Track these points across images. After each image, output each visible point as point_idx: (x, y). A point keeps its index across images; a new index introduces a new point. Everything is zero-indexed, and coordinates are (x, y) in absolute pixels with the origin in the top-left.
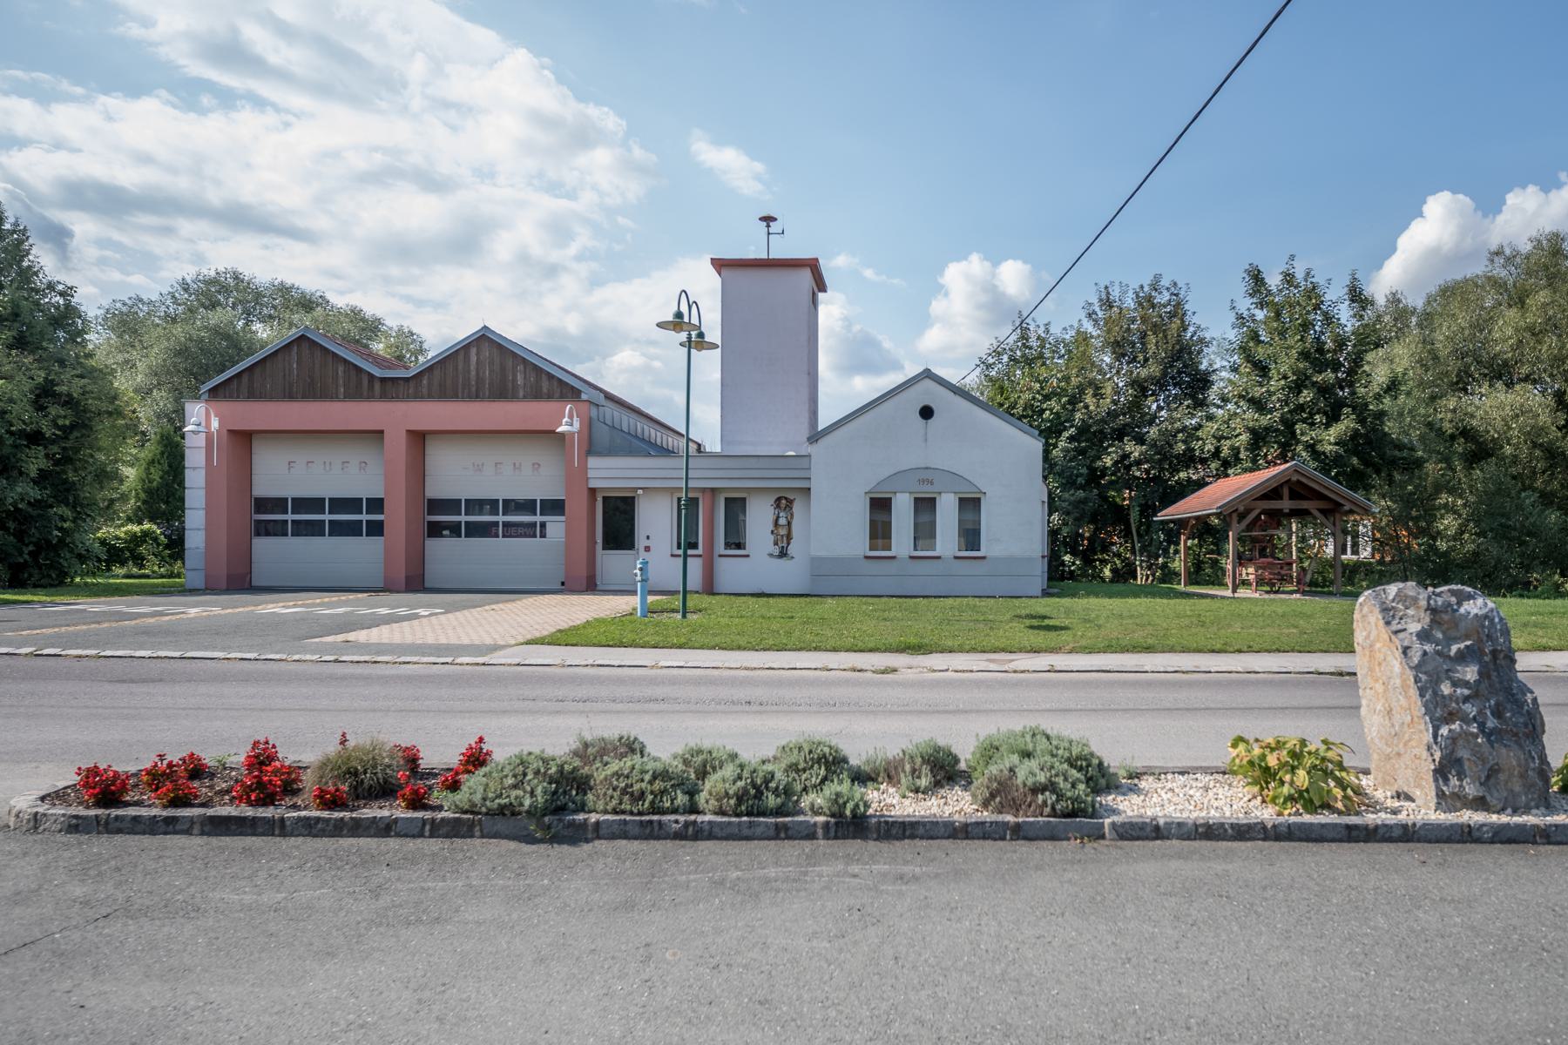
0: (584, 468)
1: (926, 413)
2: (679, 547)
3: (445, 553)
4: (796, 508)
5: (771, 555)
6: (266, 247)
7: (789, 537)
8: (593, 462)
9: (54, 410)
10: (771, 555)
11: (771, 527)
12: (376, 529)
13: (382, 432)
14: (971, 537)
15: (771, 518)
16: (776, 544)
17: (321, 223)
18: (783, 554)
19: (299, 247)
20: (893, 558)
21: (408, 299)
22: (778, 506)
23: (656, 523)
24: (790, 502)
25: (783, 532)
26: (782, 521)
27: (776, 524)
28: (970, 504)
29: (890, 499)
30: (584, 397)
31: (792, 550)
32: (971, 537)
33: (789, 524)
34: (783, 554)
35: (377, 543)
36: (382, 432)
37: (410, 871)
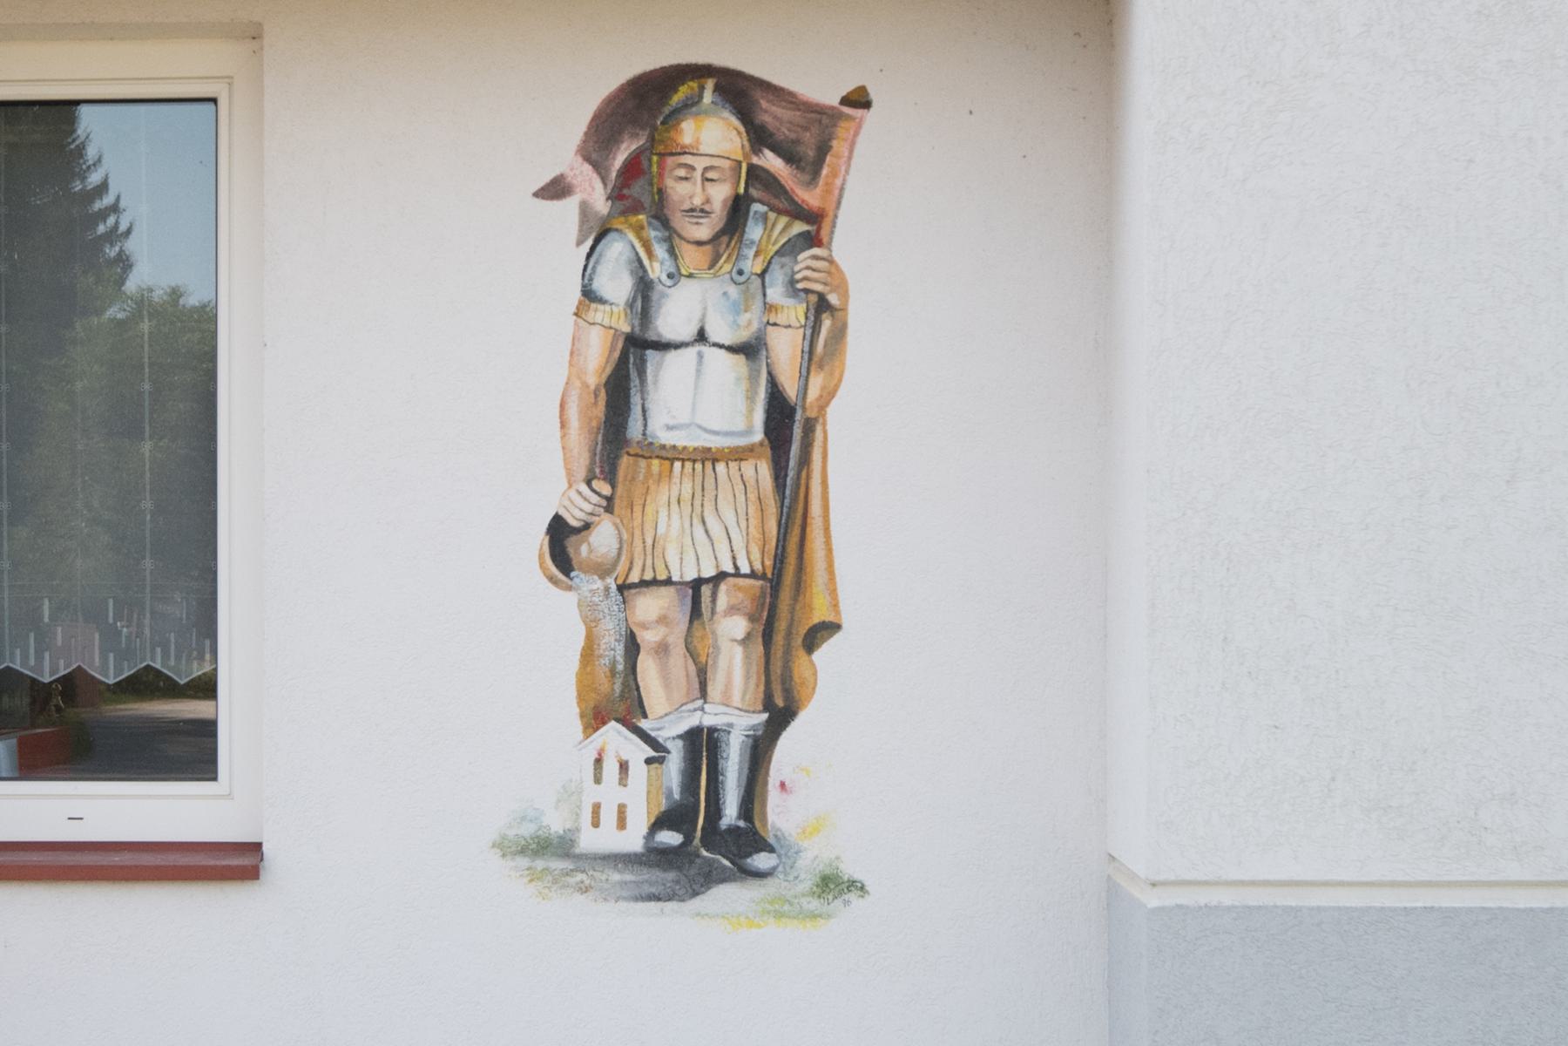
4: (880, 201)
5: (548, 851)
7: (785, 607)
10: (548, 851)
11: (551, 481)
13: (256, 848)
15: (554, 359)
16: (614, 702)
18: (709, 836)
20: (236, 863)
22: (638, 195)
24: (793, 144)
25: (701, 531)
26: (698, 400)
27: (614, 428)
31: (815, 790)
33: (786, 429)
34: (709, 836)
36: (256, 848)
37: (654, 589)
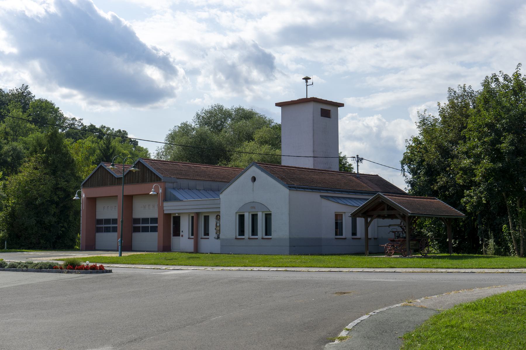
0: (162, 207)
1: (254, 179)
2: (192, 235)
3: (139, 237)
6: (377, 46)
8: (165, 204)
9: (59, 193)
12: (115, 230)
14: (268, 232)
15: (215, 223)
17: (410, 25)
19: (395, 43)
21: (462, 64)
23: (185, 225)
26: (218, 225)
28: (268, 217)
29: (257, 214)
30: (162, 181)
32: (268, 232)
35: (155, 234)
